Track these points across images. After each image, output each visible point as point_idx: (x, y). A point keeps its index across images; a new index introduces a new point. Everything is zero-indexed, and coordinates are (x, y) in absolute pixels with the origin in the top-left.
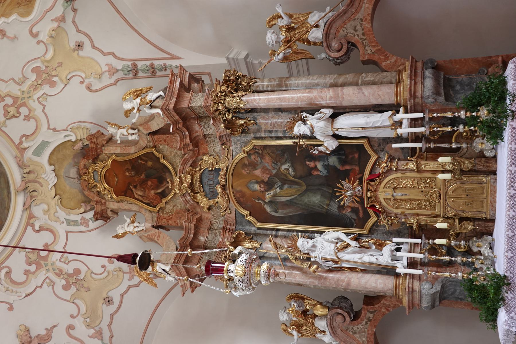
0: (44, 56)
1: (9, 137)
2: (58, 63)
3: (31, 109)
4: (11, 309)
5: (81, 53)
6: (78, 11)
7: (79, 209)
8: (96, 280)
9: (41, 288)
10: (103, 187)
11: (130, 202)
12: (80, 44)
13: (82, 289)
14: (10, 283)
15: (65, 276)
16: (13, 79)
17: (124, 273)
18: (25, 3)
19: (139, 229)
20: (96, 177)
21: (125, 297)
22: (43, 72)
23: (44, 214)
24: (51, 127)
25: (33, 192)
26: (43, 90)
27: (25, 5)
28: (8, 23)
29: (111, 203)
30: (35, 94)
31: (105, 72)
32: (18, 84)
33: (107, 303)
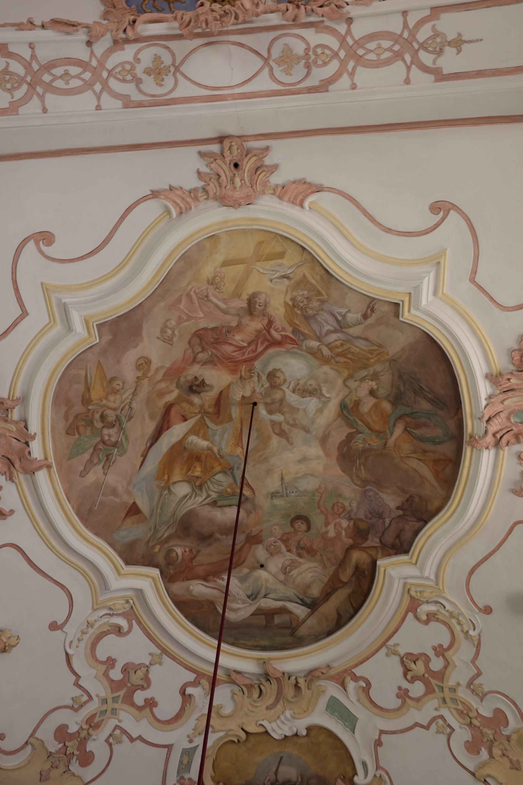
1: (367, 658)
2: (518, 761)
4: (54, 626)
9: (74, 684)
13: (48, 765)
15: (83, 734)
16: (479, 674)
22: (498, 730)
24: (384, 737)
25: (258, 691)
26: (460, 728)
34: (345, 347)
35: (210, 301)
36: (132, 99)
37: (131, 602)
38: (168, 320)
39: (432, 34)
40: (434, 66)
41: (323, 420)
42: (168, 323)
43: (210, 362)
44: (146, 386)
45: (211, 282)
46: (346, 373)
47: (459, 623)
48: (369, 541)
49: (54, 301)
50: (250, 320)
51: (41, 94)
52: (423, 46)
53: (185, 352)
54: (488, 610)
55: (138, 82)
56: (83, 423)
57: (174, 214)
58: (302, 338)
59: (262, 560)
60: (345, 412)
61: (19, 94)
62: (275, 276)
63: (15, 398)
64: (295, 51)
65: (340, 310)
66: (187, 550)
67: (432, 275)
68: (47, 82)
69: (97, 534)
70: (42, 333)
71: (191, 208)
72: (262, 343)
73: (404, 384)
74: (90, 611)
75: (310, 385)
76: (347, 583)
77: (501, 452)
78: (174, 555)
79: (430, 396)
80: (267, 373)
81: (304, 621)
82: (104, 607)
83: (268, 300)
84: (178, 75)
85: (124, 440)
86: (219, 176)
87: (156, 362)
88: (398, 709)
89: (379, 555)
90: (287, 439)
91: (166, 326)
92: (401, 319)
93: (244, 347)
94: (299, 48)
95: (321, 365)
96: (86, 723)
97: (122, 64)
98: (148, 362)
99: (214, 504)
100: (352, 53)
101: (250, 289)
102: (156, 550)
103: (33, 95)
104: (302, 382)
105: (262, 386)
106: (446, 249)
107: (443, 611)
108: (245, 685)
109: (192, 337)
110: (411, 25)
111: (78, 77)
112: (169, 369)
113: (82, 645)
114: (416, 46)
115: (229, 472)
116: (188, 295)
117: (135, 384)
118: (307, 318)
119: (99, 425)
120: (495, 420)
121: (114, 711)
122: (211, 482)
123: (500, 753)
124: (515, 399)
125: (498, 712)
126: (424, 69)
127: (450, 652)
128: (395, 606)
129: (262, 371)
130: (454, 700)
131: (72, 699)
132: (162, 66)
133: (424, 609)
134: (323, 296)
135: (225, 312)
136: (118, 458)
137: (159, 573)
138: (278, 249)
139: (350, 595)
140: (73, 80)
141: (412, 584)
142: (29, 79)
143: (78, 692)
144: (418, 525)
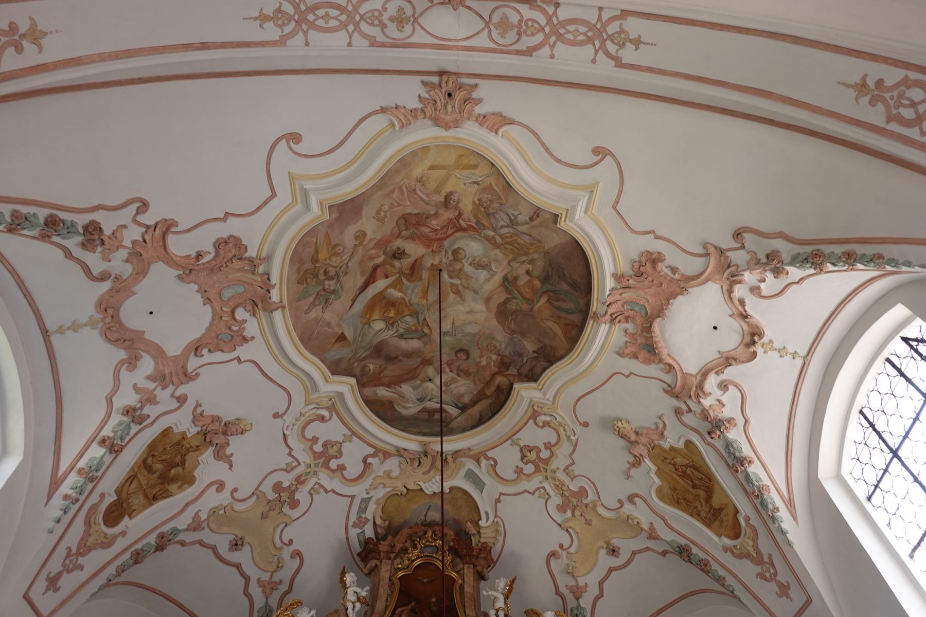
0: (602, 505)
1: (497, 446)
2: (591, 520)
3: (530, 478)
4: (276, 416)
5: (603, 552)
6: (662, 558)
7: (381, 518)
8: (274, 529)
10: (415, 558)
11: (389, 599)
12: (616, 553)
13: (268, 508)
14: (309, 419)
15: (293, 488)
16: (573, 463)
17: (273, 573)
18: (675, 496)
19: (350, 610)
20: (429, 549)
21: (234, 570)
22: (580, 500)
23: (385, 471)
24: (502, 497)
25: (418, 462)
26: (555, 496)
27: (673, 496)
28: (648, 473)
29: (389, 568)
30: (550, 486)
31: (577, 581)
32: (566, 468)
33: (234, 542)
34: (513, 239)
35: (417, 194)
36: (377, 40)
37: (333, 400)
38: (382, 205)
39: (619, 30)
40: (615, 55)
41: (489, 287)
42: (383, 208)
43: (411, 238)
44: (360, 251)
45: (419, 180)
46: (511, 257)
47: (565, 430)
48: (510, 371)
49: (297, 187)
50: (445, 211)
51: (305, 30)
52: (610, 37)
53: (392, 229)
54: (586, 425)
55: (383, 26)
56: (311, 276)
57: (397, 127)
58: (482, 228)
59: (431, 376)
60: (506, 283)
61: (288, 29)
62: (469, 181)
63: (262, 257)
64: (511, 20)
65: (513, 212)
66: (377, 366)
67: (586, 199)
68: (311, 20)
69: (313, 354)
70: (286, 210)
71: (410, 124)
72: (452, 228)
73: (552, 269)
74: (303, 405)
75: (484, 262)
76: (490, 396)
77: (614, 327)
78: (368, 369)
79: (569, 281)
80: (452, 249)
81: (455, 418)
82: (313, 403)
83: (460, 198)
84: (416, 25)
85: (339, 288)
86: (436, 102)
87: (370, 235)
88: (514, 480)
89: (516, 380)
90: (461, 297)
91: (381, 210)
92: (558, 226)
93: (438, 230)
94: (514, 18)
95: (494, 249)
96: (295, 481)
97: (372, 11)
98: (364, 234)
99: (401, 336)
100: (555, 31)
101: (448, 188)
102: (355, 365)
103: (298, 31)
104: (477, 259)
105: (448, 258)
106: (599, 182)
107: (554, 421)
108: (410, 459)
109: (400, 218)
110: (604, 19)
111: (336, 18)
112: (380, 240)
113: (296, 428)
114: (605, 37)
115: (415, 316)
116: (400, 188)
117: (352, 250)
118: (488, 215)
119: (322, 277)
120: (613, 305)
121: (315, 473)
122: (401, 321)
123: (579, 514)
124: (630, 294)
125: (582, 488)
126: (608, 55)
127: (555, 448)
128: (522, 414)
129: (449, 248)
130: (554, 478)
131: (286, 464)
132: (404, 16)
133: (542, 419)
134: (502, 200)
135: (427, 203)
136: (334, 301)
137: (356, 381)
138: (474, 162)
139: (490, 405)
140: (332, 20)
141: (536, 402)
142: (296, 17)
143: (291, 460)
144: (546, 364)
